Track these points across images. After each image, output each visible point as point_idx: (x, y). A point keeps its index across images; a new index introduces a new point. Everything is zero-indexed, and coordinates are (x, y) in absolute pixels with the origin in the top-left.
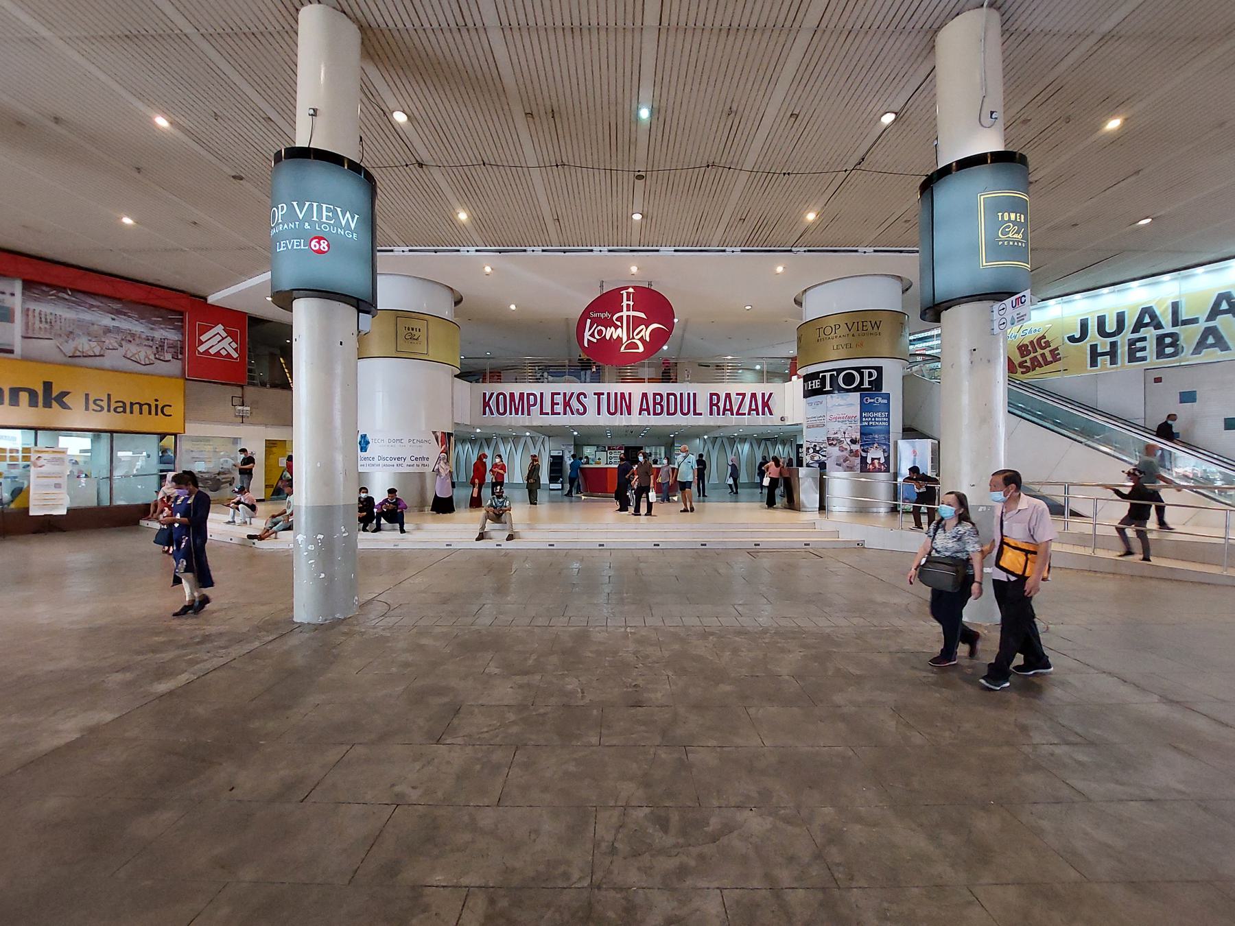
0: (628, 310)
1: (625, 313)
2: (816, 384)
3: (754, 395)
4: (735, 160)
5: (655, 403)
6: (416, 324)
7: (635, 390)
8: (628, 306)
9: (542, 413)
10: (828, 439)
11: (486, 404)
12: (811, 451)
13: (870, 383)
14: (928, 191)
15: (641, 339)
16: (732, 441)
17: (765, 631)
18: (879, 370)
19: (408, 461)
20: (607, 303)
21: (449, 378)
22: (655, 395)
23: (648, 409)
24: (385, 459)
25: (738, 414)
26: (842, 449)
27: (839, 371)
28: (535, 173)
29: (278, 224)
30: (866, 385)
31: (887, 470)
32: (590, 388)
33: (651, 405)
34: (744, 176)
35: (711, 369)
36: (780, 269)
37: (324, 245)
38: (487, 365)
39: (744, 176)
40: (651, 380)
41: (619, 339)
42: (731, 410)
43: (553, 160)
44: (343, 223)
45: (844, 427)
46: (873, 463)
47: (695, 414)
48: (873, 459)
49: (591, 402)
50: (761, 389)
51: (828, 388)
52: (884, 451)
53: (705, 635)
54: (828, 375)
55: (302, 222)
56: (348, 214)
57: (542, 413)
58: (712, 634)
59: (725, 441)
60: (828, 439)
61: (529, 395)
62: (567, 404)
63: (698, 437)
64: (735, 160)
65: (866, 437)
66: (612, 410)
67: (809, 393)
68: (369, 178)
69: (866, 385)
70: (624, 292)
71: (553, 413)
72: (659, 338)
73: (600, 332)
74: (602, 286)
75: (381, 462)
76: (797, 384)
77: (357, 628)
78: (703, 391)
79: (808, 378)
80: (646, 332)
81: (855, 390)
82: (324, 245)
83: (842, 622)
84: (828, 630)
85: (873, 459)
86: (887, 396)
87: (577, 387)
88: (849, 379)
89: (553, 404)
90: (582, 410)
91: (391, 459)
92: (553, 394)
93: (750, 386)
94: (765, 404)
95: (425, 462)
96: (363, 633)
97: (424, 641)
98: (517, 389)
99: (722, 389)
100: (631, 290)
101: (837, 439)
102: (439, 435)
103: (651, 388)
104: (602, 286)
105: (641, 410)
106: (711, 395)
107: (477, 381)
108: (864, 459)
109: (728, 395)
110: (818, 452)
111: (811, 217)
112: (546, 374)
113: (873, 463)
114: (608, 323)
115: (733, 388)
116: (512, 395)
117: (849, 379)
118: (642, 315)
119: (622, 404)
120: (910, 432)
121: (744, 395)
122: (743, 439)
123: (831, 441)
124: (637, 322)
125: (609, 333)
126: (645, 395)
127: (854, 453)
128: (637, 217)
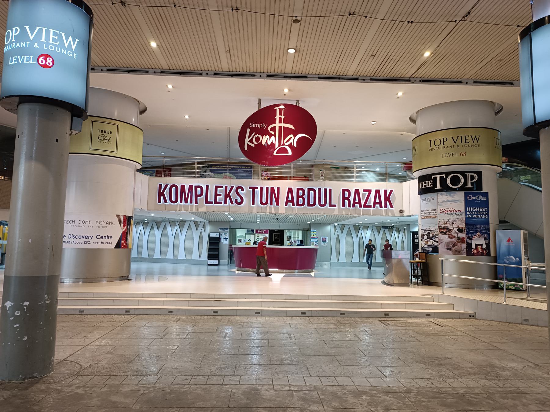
0: (280, 122)
1: (277, 125)
2: (429, 184)
3: (378, 192)
4: (371, 11)
5: (298, 197)
6: (108, 127)
7: (283, 186)
8: (280, 119)
9: (207, 202)
10: (440, 228)
11: (161, 194)
12: (426, 237)
13: (472, 184)
14: (527, 38)
15: (290, 146)
16: (357, 228)
17: (409, 391)
18: (479, 173)
19: (94, 239)
20: (262, 118)
21: (132, 172)
22: (298, 190)
23: (292, 201)
24: (74, 237)
25: (365, 206)
26: (451, 237)
27: (447, 174)
28: (215, 14)
29: (11, 43)
30: (469, 186)
31: (488, 254)
32: (247, 183)
33: (297, 198)
34: (377, 22)
35: (341, 171)
36: (400, 94)
37: (49, 61)
38: (164, 162)
39: (377, 22)
40: (295, 178)
41: (273, 145)
42: (359, 203)
43: (230, 5)
44: (66, 45)
45: (452, 218)
46: (476, 249)
47: (330, 205)
48: (476, 245)
49: (245, 193)
50: (383, 187)
51: (438, 187)
52: (485, 239)
53: (358, 394)
54: (438, 177)
55: (32, 43)
56: (70, 39)
57: (207, 202)
58: (364, 393)
59: (375, 229)
60: (440, 228)
61: (196, 187)
62: (227, 195)
63: (330, 224)
64: (371, 11)
65: (473, 227)
66: (264, 201)
67: (423, 191)
68: (88, 11)
69: (469, 186)
70: (277, 108)
71: (216, 202)
72: (303, 147)
73: (257, 139)
74: (259, 103)
75: (71, 240)
76: (413, 185)
77: (53, 386)
78: (337, 187)
79: (421, 179)
80: (294, 140)
81: (461, 189)
82: (49, 61)
83: (472, 383)
84: (462, 391)
85: (476, 245)
86: (486, 195)
87: (235, 182)
88: (455, 180)
89: (216, 195)
90: (239, 200)
91: (80, 237)
92: (217, 187)
93: (368, 183)
94: (387, 199)
95: (109, 240)
96: (59, 391)
97: (114, 398)
98: (187, 182)
99: (346, 185)
100: (282, 107)
101: (446, 228)
102: (122, 218)
103: (295, 185)
104: (259, 103)
105: (287, 201)
106: (344, 191)
107: (151, 175)
108: (469, 246)
109: (357, 191)
110: (431, 238)
111: (427, 54)
112: (208, 171)
113: (476, 249)
114: (264, 132)
115: (361, 186)
116: (183, 187)
117: (455, 180)
118: (291, 127)
119: (273, 196)
120: (504, 223)
121: (370, 191)
122: (366, 227)
123: (444, 230)
124: (287, 132)
125: (265, 140)
126: (290, 190)
127: (462, 240)
128: (292, 51)
